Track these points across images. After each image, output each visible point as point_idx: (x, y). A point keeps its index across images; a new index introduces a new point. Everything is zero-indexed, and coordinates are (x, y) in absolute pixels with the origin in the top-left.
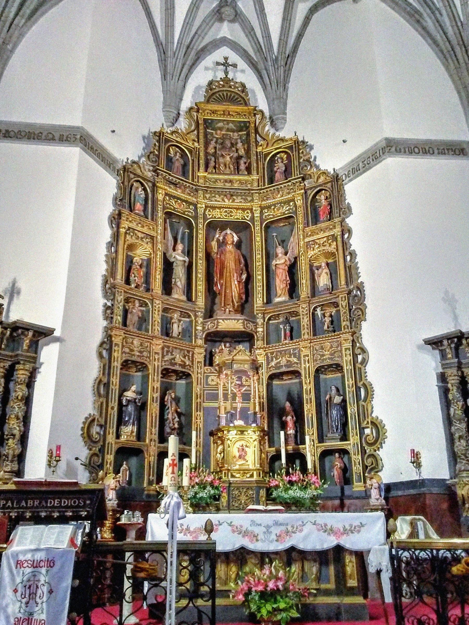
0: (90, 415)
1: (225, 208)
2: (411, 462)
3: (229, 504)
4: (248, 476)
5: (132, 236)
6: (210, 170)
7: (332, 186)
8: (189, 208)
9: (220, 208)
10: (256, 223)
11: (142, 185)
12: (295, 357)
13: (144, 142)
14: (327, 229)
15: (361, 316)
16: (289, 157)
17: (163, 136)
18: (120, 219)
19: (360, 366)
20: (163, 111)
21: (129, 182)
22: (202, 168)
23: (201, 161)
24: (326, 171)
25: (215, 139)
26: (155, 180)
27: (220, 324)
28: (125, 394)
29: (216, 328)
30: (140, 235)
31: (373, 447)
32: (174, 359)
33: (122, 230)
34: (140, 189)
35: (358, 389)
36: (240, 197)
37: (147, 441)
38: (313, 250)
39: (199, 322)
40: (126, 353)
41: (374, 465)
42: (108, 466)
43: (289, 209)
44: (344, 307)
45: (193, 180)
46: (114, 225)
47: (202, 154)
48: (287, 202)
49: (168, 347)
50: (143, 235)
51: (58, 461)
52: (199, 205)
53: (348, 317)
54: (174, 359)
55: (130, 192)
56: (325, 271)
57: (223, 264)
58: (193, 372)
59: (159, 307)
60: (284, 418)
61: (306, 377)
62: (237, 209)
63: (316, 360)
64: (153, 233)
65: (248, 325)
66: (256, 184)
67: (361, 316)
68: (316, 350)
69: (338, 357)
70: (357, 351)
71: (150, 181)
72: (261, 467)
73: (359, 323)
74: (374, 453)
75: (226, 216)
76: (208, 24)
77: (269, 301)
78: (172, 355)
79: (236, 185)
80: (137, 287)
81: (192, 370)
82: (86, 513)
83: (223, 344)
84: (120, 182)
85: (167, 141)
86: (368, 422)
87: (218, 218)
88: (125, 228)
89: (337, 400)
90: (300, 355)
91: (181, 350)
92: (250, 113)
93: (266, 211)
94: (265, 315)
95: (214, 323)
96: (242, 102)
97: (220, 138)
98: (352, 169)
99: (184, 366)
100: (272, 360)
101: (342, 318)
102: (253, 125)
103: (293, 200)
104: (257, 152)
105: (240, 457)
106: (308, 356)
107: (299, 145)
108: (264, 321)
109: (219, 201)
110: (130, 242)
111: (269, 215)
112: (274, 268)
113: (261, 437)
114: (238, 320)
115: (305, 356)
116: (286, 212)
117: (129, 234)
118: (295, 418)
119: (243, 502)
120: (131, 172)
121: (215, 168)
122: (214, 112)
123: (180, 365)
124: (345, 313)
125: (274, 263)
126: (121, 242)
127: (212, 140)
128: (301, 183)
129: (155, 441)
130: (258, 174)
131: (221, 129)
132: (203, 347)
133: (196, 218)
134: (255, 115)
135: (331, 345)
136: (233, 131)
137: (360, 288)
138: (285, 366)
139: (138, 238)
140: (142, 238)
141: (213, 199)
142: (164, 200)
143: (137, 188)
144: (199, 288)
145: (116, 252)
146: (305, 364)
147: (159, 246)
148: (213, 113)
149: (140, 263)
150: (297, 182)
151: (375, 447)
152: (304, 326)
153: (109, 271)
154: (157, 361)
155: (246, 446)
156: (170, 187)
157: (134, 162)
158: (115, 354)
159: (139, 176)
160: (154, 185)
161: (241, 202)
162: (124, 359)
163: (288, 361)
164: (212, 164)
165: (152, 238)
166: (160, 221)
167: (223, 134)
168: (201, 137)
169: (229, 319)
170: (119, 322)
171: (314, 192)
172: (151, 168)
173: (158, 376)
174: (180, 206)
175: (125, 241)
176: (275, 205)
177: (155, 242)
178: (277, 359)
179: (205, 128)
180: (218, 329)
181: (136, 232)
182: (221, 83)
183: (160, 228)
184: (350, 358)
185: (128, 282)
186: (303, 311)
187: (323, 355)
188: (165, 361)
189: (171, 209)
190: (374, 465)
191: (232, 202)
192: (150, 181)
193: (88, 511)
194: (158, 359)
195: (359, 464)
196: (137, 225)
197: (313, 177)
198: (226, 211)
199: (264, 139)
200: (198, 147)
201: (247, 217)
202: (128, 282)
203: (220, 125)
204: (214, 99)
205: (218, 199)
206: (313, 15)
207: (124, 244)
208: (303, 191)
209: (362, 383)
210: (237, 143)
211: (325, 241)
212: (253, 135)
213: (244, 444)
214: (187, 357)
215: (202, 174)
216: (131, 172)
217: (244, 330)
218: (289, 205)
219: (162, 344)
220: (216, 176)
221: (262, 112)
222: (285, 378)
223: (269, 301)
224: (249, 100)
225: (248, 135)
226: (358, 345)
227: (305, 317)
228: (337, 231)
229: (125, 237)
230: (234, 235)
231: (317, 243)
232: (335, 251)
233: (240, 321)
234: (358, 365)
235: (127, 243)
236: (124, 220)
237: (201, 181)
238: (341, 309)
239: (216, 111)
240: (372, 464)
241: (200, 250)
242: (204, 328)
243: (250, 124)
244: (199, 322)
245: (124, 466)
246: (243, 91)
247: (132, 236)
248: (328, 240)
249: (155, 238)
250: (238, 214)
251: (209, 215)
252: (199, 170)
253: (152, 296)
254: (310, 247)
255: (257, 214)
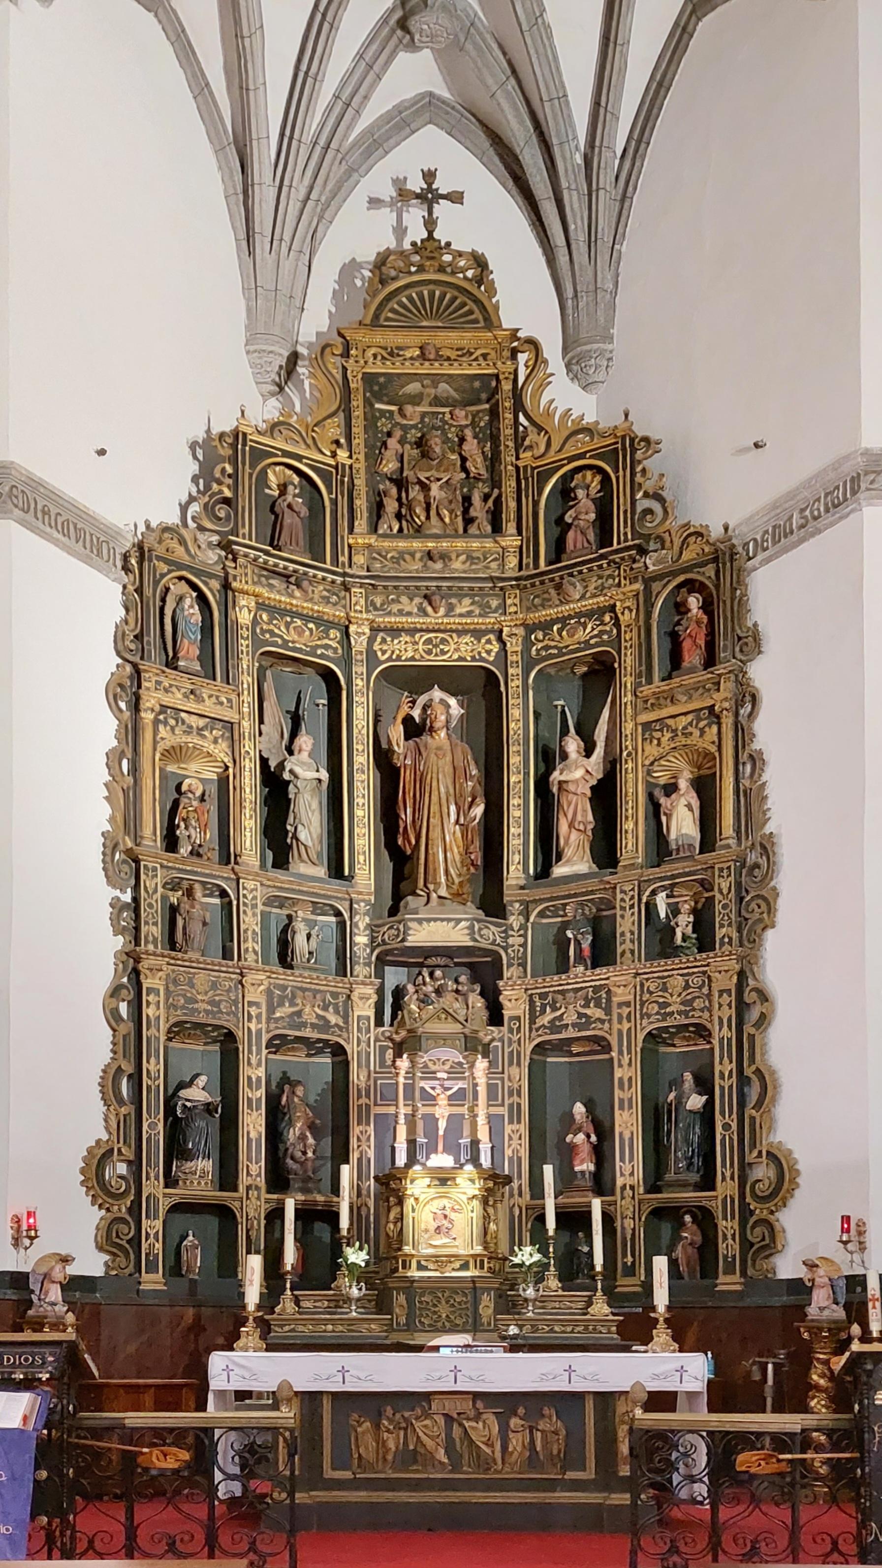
0: (98, 1142)
1: (428, 631)
2: (841, 1241)
3: (475, 1297)
4: (457, 1265)
5: (173, 729)
6: (383, 528)
7: (717, 572)
8: (328, 637)
9: (412, 631)
10: (511, 671)
11: (194, 587)
12: (598, 1005)
13: (195, 457)
14: (697, 689)
15: (765, 915)
16: (606, 480)
17: (244, 444)
18: (139, 686)
19: (752, 1031)
20: (248, 352)
21: (156, 583)
22: (361, 524)
23: (357, 502)
24: (703, 531)
25: (398, 433)
26: (227, 574)
27: (410, 932)
28: (183, 1093)
29: (403, 940)
30: (194, 721)
31: (767, 1205)
32: (299, 1014)
33: (147, 717)
34: (188, 602)
35: (743, 1081)
36: (467, 601)
37: (242, 1188)
38: (659, 745)
39: (362, 926)
40: (175, 1007)
41: (767, 1241)
42: (152, 1240)
43: (602, 632)
44: (725, 891)
45: (335, 561)
46: (123, 705)
47: (360, 482)
48: (596, 613)
49: (284, 988)
50: (202, 722)
51: (32, 1238)
52: (352, 629)
53: (733, 916)
54: (299, 1014)
55: (162, 609)
56: (683, 801)
57: (420, 780)
58: (347, 1041)
59: (255, 898)
60: (569, 1138)
61: (621, 1052)
62: (461, 633)
63: (649, 1016)
64: (230, 715)
65: (484, 932)
66: (512, 562)
67: (765, 915)
68: (651, 993)
69: (702, 1010)
70: (749, 997)
71: (211, 576)
72: (485, 1248)
73: (759, 931)
74: (772, 1218)
75: (429, 652)
76: (370, 67)
77: (544, 872)
78: (292, 1004)
79: (458, 565)
80: (196, 853)
81: (345, 1035)
82: (48, 1376)
83: (425, 972)
84: (131, 588)
85: (259, 454)
86: (760, 1152)
87: (406, 660)
88: (153, 710)
89: (696, 1102)
90: (609, 1000)
91: (315, 992)
92: (499, 350)
93: (541, 637)
94: (531, 906)
95: (398, 929)
96: (477, 315)
97: (414, 427)
98: (774, 527)
99: (324, 1026)
100: (543, 1012)
101: (717, 920)
102: (507, 386)
103: (612, 609)
104: (517, 468)
105: (438, 1230)
106: (628, 1004)
107: (634, 451)
108: (527, 920)
109: (409, 614)
110: (167, 744)
111: (547, 648)
112: (555, 790)
113: (487, 1190)
114: (458, 921)
115: (620, 1005)
116: (592, 642)
117: (166, 723)
118: (593, 1138)
119: (444, 1316)
120: (159, 558)
121: (399, 516)
122: (393, 353)
123: (313, 1026)
124: (725, 907)
125: (556, 776)
126: (146, 746)
127: (389, 434)
128: (634, 561)
129: (257, 1188)
130: (520, 533)
131: (416, 399)
132: (371, 983)
133: (347, 661)
134: (514, 352)
135: (687, 982)
136: (452, 404)
137: (767, 848)
138: (574, 1025)
139: (189, 730)
140: (200, 729)
141: (395, 608)
142: (255, 622)
143: (180, 599)
144: (360, 843)
145: (135, 770)
146: (620, 1022)
147: (248, 746)
148: (391, 354)
149: (198, 793)
150: (622, 559)
151: (771, 1205)
152: (623, 934)
153: (120, 819)
154: (254, 1020)
155: (453, 1209)
156: (271, 586)
157: (166, 529)
158: (149, 1011)
159: (180, 566)
160: (226, 586)
161: (469, 614)
162: (172, 1021)
163: (580, 1015)
164: (391, 506)
165: (230, 726)
166: (247, 680)
167: (424, 415)
168: (358, 429)
169: (435, 920)
170: (155, 939)
171: (670, 587)
172: (215, 538)
173: (259, 1052)
174: (300, 633)
175: (155, 743)
176: (563, 620)
177: (236, 737)
178: (554, 1009)
179: (368, 403)
180: (407, 944)
181: (183, 715)
182: (416, 258)
183: (249, 699)
184: (728, 1013)
185: (171, 843)
186: (622, 900)
187: (666, 1005)
188: (277, 1020)
189: (274, 644)
190: (767, 1241)
191: (446, 615)
192: (211, 576)
193: (51, 1373)
194: (259, 1016)
195: (734, 1240)
196: (185, 696)
197: (668, 544)
198: (429, 641)
199: (540, 429)
200: (348, 462)
201: (489, 652)
202: (171, 843)
203: (413, 388)
204: (393, 311)
205: (407, 609)
206: (699, 19)
207: (155, 749)
208: (638, 586)
209: (753, 1068)
210: (462, 440)
211: (691, 724)
212: (509, 416)
213: (448, 1205)
214: (331, 1009)
215: (361, 537)
216: (159, 558)
217: (471, 944)
218: (603, 623)
219: (266, 983)
220: (402, 544)
221: (533, 344)
222: (575, 1049)
223: (544, 872)
224: (496, 307)
225: (494, 413)
226: (751, 982)
227: (628, 912)
228: (722, 699)
229: (156, 732)
230: (452, 701)
231: (668, 726)
232: (713, 749)
233: (463, 924)
234: (748, 1029)
235: (160, 747)
236: (148, 689)
237: (360, 559)
238: (718, 896)
239: (398, 348)
240: (763, 1239)
241: (360, 748)
242: (373, 939)
243: (498, 381)
244: (362, 926)
245: (191, 1238)
246: (479, 280)
247: (173, 729)
248: (699, 720)
249: (236, 727)
250: (463, 648)
251: (384, 652)
252: (351, 530)
253: (235, 874)
254: (652, 738)
255: (514, 646)
